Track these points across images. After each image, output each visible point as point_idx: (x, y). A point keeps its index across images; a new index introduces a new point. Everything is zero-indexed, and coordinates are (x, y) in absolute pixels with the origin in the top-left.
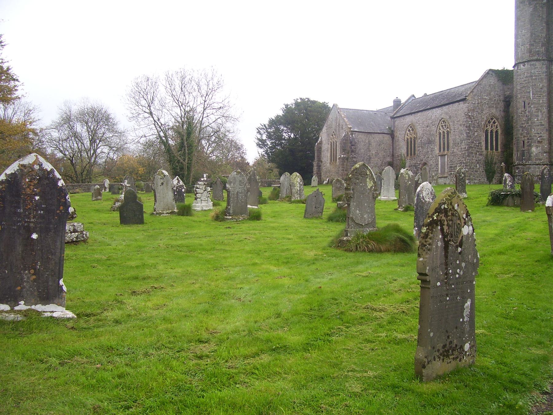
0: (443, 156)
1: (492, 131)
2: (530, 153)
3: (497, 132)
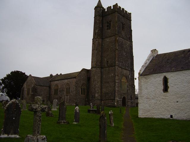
0: (67, 96)
1: (83, 88)
2: (95, 96)
3: (85, 89)
